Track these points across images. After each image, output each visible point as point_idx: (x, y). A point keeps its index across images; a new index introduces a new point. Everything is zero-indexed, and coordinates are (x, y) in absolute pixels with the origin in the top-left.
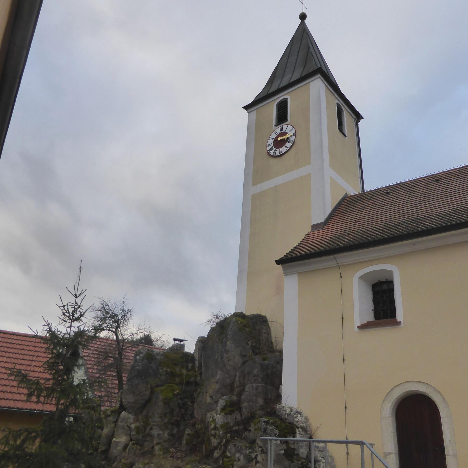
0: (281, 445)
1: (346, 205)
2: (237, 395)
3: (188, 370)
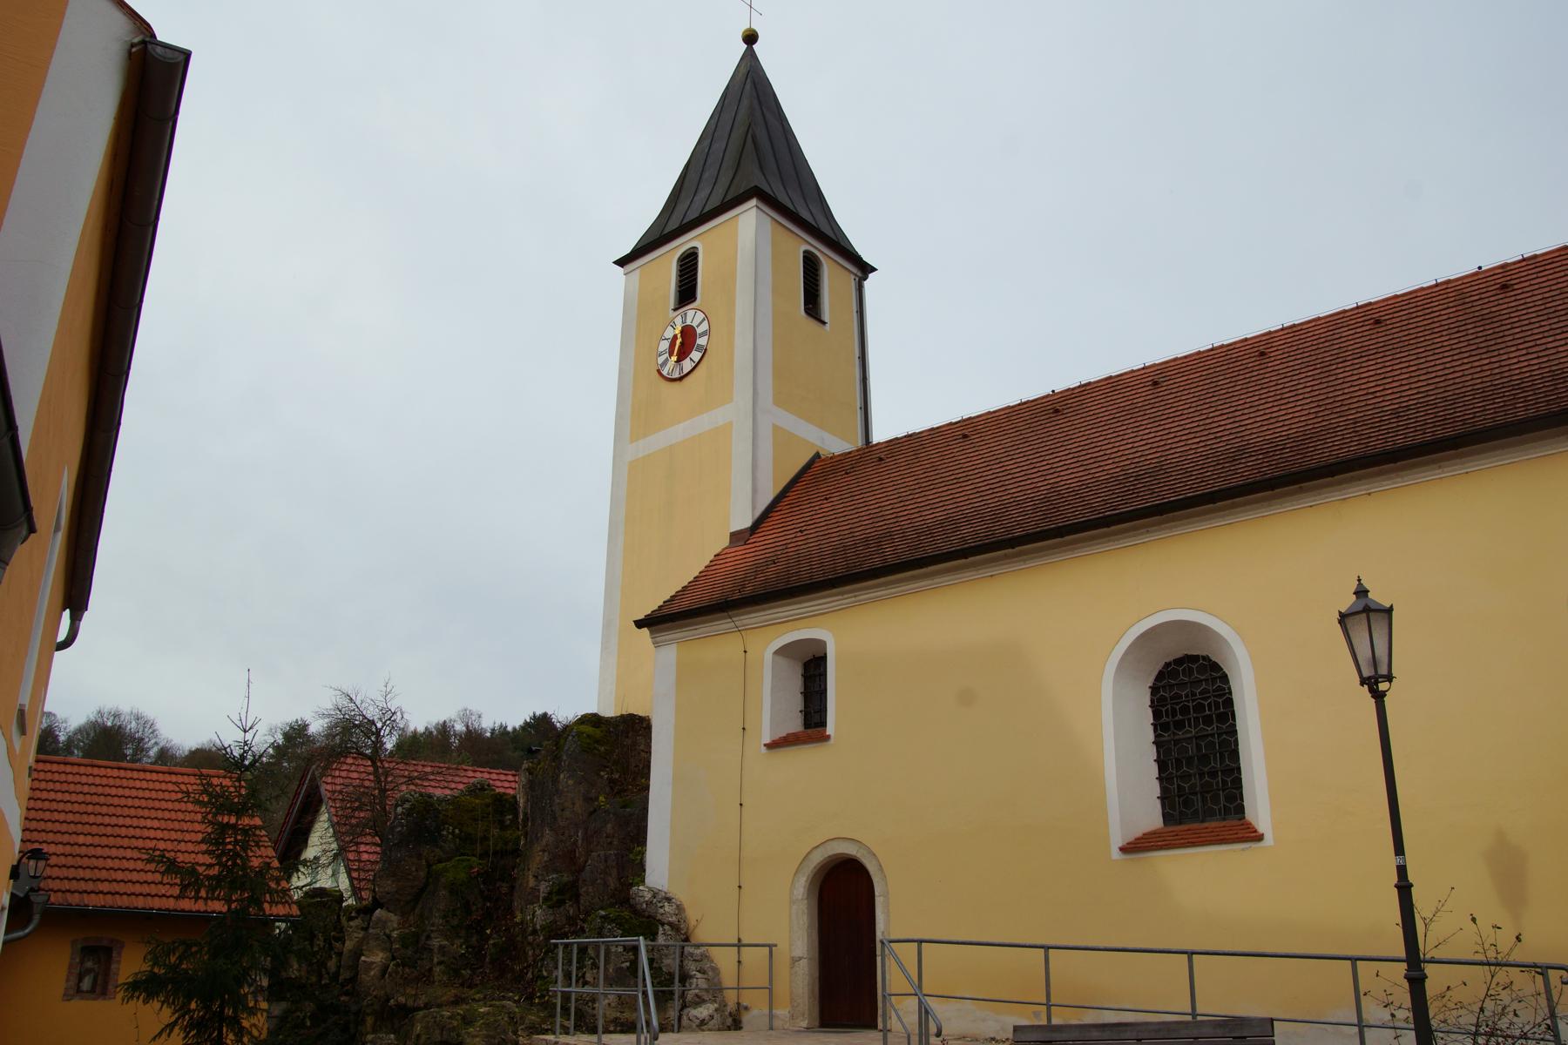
1: (815, 476)
3: (503, 827)
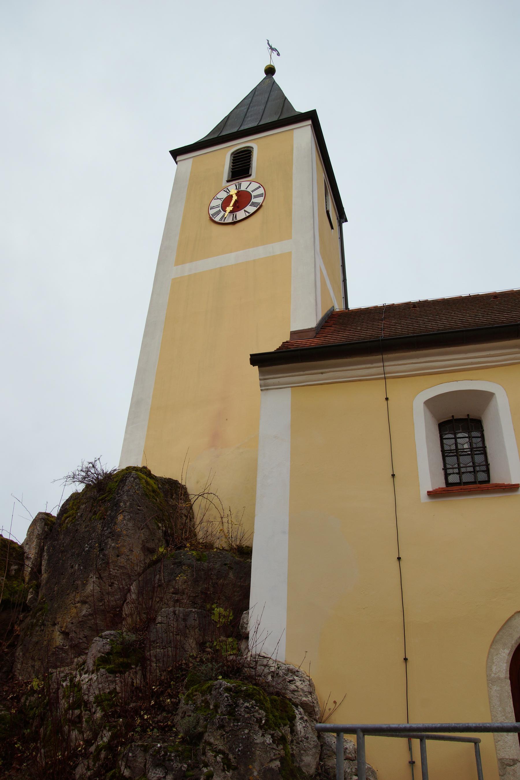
0: (275, 746)
2: (134, 630)
